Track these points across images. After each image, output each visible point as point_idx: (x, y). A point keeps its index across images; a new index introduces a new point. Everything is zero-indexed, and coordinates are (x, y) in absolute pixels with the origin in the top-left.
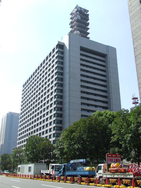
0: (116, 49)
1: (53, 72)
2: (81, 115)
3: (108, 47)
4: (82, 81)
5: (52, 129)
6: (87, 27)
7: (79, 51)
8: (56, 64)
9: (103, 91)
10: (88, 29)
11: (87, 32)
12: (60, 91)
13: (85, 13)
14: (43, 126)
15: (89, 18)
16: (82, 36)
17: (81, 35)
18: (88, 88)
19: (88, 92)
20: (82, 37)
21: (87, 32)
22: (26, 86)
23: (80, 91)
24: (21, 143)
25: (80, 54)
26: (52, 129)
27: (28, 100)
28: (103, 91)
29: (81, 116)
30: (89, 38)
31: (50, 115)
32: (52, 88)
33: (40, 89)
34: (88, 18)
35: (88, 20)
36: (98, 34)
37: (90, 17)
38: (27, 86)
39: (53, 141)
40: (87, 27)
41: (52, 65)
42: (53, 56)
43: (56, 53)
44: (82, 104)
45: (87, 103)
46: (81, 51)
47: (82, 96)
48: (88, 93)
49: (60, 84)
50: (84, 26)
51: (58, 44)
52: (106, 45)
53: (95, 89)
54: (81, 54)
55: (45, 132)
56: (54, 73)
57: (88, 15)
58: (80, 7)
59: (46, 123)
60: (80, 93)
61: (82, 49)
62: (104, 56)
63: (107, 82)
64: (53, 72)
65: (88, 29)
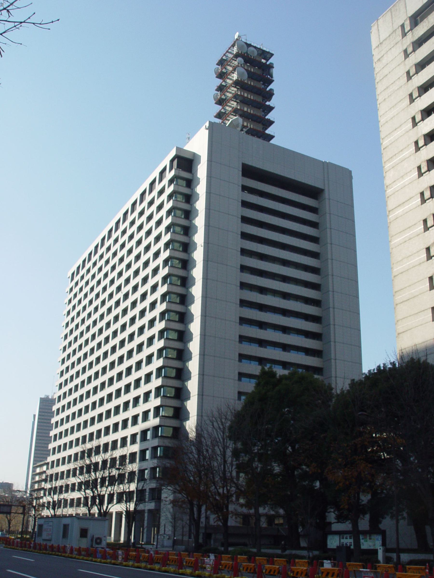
0: (350, 172)
1: (159, 223)
2: (238, 337)
3: (326, 166)
4: (243, 268)
5: (151, 414)
6: (267, 103)
7: (238, 179)
8: (167, 216)
9: (307, 301)
10: (271, 109)
11: (267, 117)
12: (177, 318)
13: (264, 61)
14: (126, 404)
15: (274, 75)
16: (251, 132)
17: (245, 130)
18: (263, 290)
19: (263, 320)
20: (253, 135)
21: (267, 117)
22: (79, 277)
23: (238, 302)
24: (59, 451)
25: (240, 188)
26: (151, 414)
27: (83, 321)
28: (307, 301)
29: (237, 378)
30: (272, 137)
31: (148, 334)
32: (154, 288)
33: (119, 289)
34: (272, 76)
35: (270, 82)
36: (297, 129)
37: (275, 72)
38: (82, 277)
39: (150, 489)
40: (267, 103)
41: (157, 203)
42: (161, 192)
43: (171, 181)
44: (242, 339)
45: (258, 302)
46: (244, 178)
47: (243, 247)
48: (262, 307)
49: (176, 331)
50: (259, 99)
51: (176, 155)
52: (323, 159)
53: (286, 296)
54: (244, 188)
55: (131, 404)
56: (161, 244)
57: (271, 66)
58: (246, 43)
59: (135, 375)
60: (239, 253)
61: (248, 171)
62: (315, 193)
63: (322, 287)
64: (159, 223)
65: (271, 109)
